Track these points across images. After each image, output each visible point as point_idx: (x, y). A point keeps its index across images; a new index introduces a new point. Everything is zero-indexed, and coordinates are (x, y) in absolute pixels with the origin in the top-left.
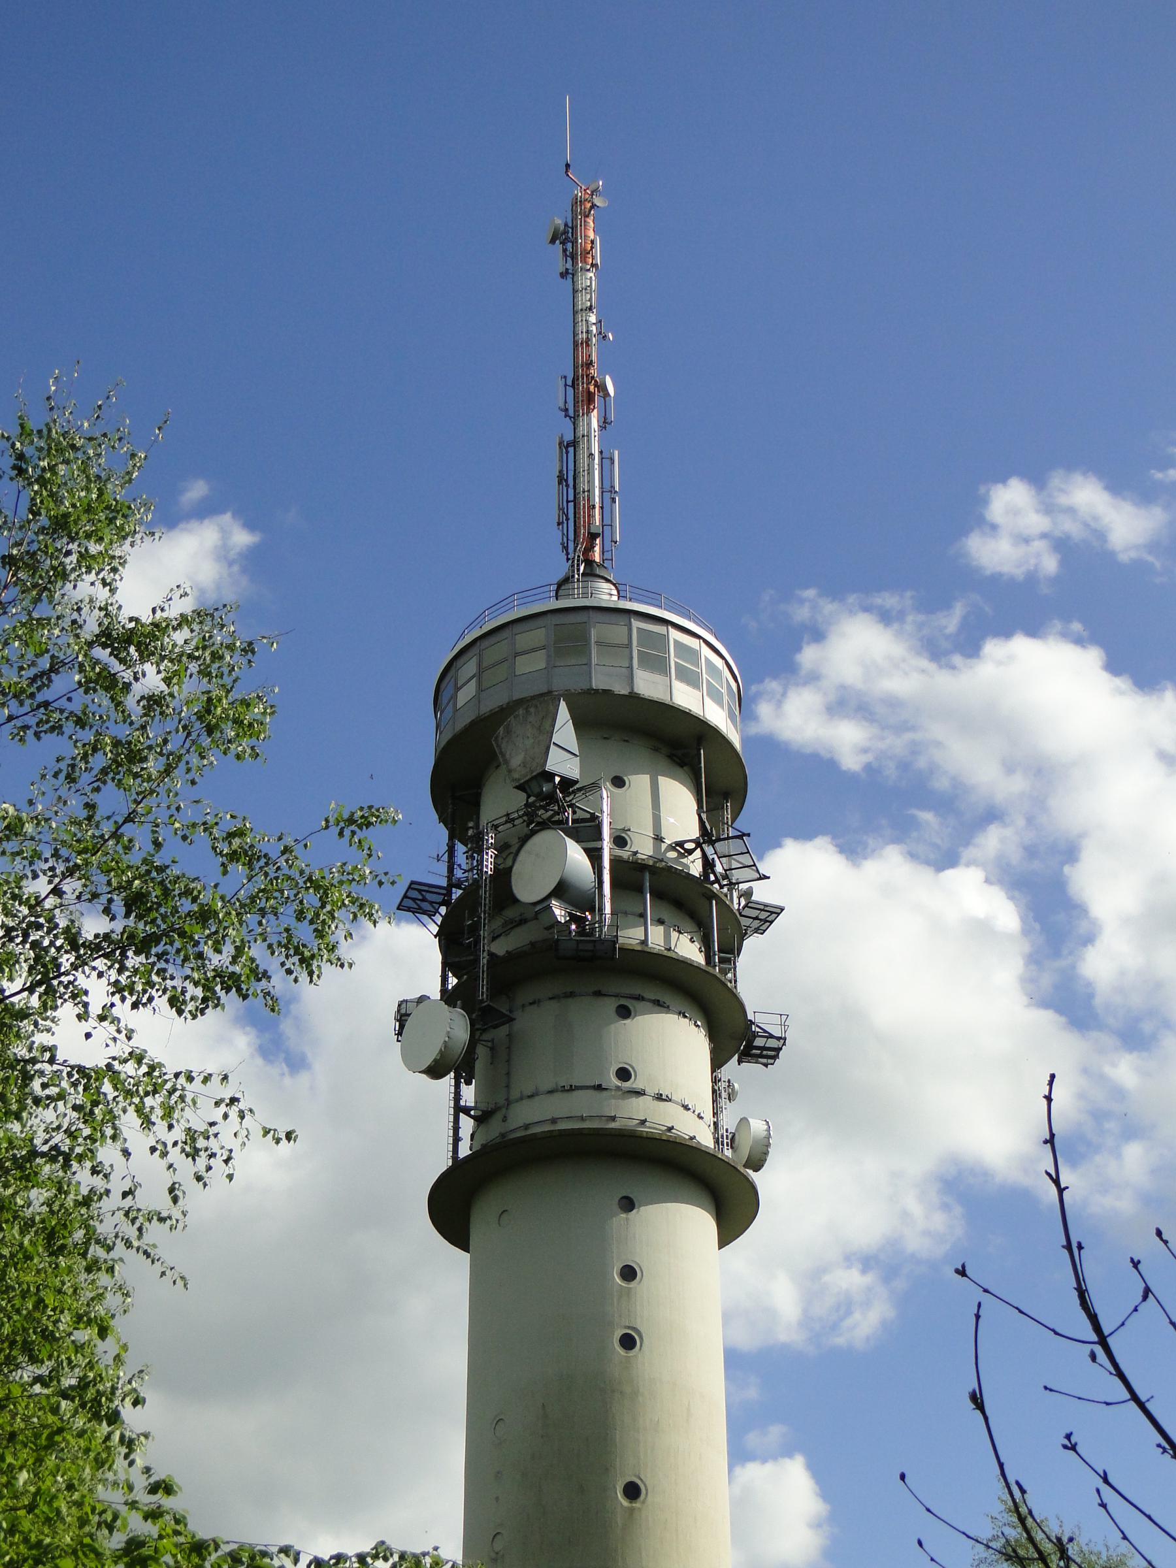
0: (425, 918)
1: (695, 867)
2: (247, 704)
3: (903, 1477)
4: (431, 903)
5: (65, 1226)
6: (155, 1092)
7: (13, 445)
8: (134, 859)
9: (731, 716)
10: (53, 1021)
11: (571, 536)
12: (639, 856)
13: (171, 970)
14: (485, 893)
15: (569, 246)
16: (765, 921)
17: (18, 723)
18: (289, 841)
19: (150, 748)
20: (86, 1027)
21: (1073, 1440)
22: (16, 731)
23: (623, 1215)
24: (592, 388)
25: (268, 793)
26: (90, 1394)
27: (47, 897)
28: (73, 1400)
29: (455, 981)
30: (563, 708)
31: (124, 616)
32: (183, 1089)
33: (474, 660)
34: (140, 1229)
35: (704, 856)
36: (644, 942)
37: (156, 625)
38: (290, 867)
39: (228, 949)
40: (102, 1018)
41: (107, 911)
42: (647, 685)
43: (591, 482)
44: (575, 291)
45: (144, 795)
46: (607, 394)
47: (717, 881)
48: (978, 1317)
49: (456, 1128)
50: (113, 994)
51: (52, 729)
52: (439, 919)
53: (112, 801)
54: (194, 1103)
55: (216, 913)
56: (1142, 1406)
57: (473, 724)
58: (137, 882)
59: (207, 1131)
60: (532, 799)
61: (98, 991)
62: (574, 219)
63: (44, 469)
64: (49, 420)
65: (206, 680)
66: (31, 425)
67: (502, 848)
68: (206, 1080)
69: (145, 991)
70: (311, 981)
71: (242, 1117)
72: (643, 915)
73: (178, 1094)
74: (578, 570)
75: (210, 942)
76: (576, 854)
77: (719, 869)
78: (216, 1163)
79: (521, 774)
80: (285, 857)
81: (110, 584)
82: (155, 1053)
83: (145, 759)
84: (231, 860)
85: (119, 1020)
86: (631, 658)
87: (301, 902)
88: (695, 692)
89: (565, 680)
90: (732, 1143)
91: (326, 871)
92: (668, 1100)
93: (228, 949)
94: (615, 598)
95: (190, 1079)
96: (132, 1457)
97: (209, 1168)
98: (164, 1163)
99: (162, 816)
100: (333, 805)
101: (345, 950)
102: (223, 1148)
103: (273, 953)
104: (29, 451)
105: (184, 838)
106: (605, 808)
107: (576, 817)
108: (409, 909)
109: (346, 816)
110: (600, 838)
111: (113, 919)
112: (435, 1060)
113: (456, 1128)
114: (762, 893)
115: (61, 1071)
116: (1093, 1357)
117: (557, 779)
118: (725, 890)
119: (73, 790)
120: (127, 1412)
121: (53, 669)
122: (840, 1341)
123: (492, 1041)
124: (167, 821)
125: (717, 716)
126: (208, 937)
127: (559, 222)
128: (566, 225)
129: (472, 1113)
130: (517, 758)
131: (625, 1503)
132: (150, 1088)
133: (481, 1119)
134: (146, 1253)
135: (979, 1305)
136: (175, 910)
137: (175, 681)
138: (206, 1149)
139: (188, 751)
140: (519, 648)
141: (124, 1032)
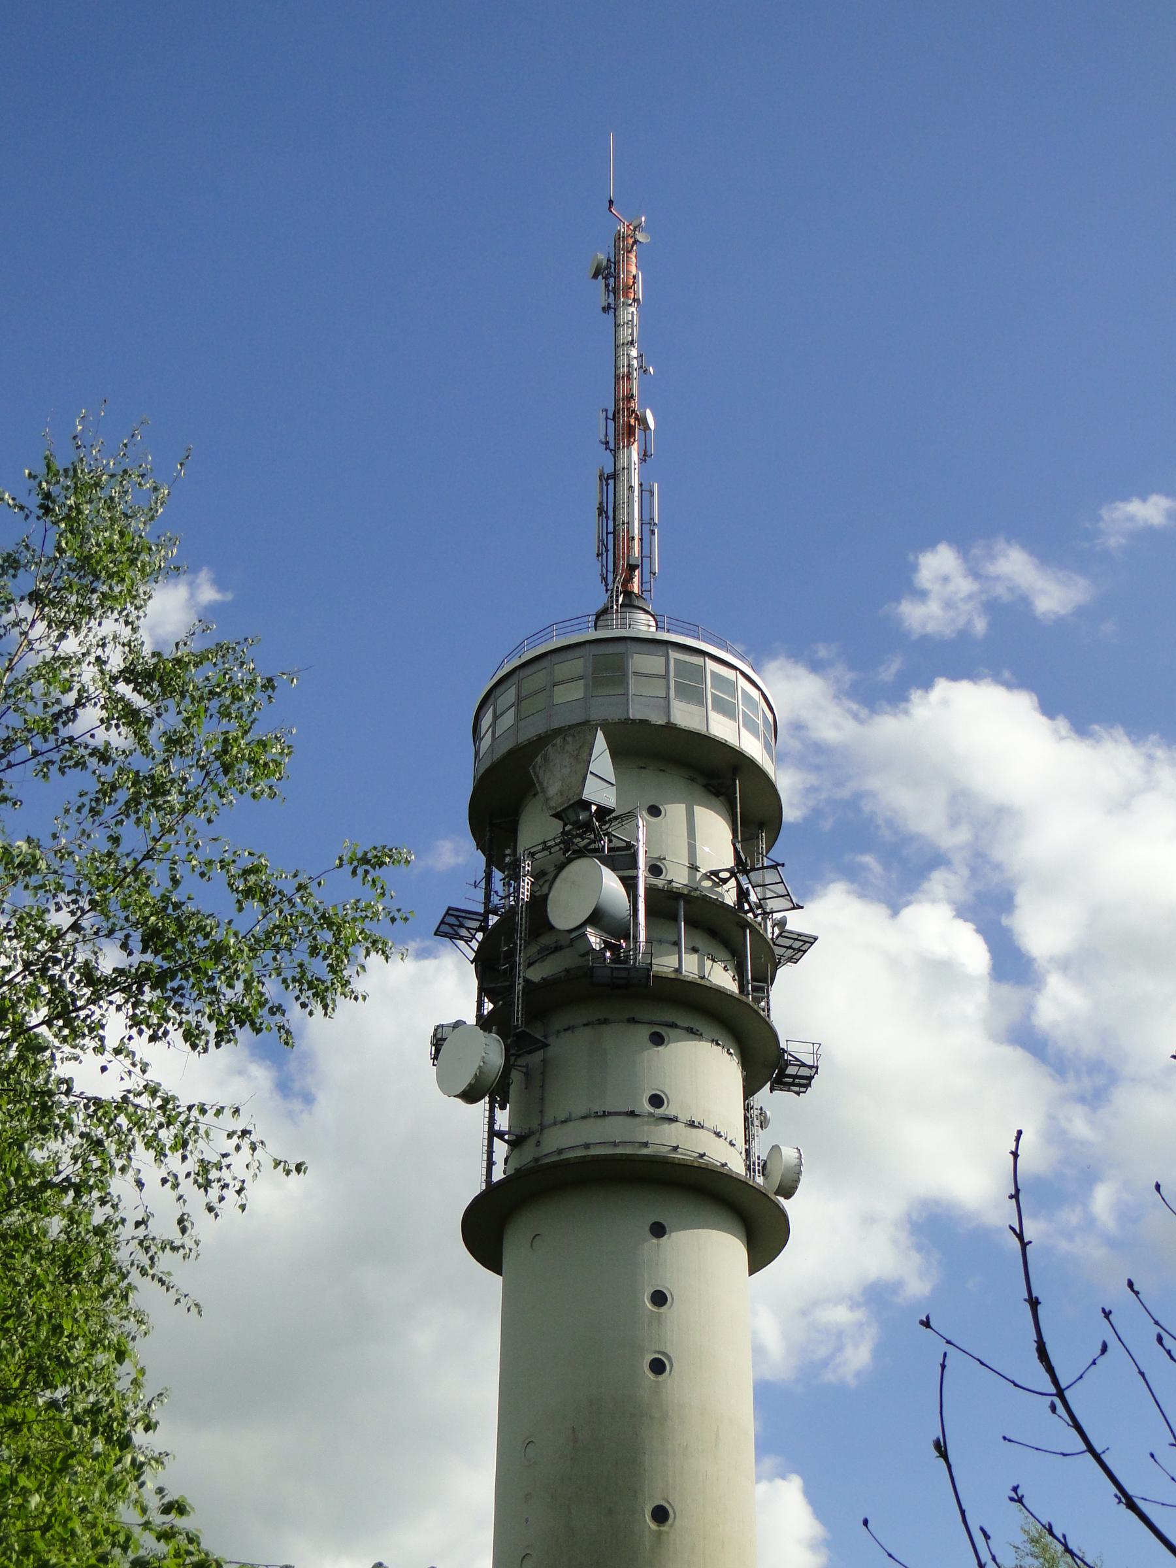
0: (461, 943)
1: (729, 896)
2: (263, 744)
3: (866, 1522)
4: (468, 929)
5: (80, 1254)
6: (169, 1124)
7: (40, 485)
8: (153, 894)
9: (767, 747)
10: (82, 1049)
11: (611, 568)
12: (674, 884)
13: (187, 1004)
14: (521, 920)
15: (612, 280)
16: (799, 950)
17: (42, 759)
18: (303, 878)
19: (173, 781)
20: (101, 1060)
21: (1020, 1492)
22: (39, 768)
23: (654, 1241)
24: (632, 422)
25: (278, 831)
26: (103, 1418)
27: (66, 932)
28: (85, 1425)
29: (491, 1006)
30: (600, 735)
31: (147, 650)
32: (197, 1121)
33: (513, 690)
34: (152, 1258)
35: (739, 885)
36: (678, 970)
37: (178, 661)
38: (305, 903)
39: (239, 986)
40: (117, 1052)
41: (124, 946)
42: (684, 715)
43: (630, 514)
44: (617, 325)
45: (165, 830)
46: (647, 428)
47: (751, 910)
48: (943, 1366)
49: (490, 1152)
50: (131, 1027)
51: (77, 764)
52: (475, 945)
53: (134, 838)
54: (207, 1134)
55: (228, 947)
56: (1097, 1457)
57: (511, 753)
58: (153, 918)
59: (220, 1162)
60: (568, 828)
61: (116, 1025)
62: (617, 254)
63: (70, 507)
64: (76, 459)
65: (224, 721)
66: (59, 464)
67: (539, 876)
68: (219, 1112)
69: (160, 1026)
70: (326, 1014)
71: (254, 1149)
72: (677, 944)
73: (191, 1126)
74: (617, 601)
75: (223, 977)
76: (611, 882)
77: (753, 898)
78: (230, 1194)
79: (558, 803)
80: (300, 894)
81: (132, 623)
82: (168, 1086)
83: (168, 792)
84: (247, 897)
85: (134, 1054)
86: (668, 688)
87: (315, 938)
88: (732, 722)
89: (604, 709)
90: (764, 1171)
91: (340, 907)
93: (239, 986)
94: (653, 629)
95: (203, 1111)
96: (142, 1478)
97: (222, 1199)
98: (174, 1195)
99: (180, 852)
100: (347, 843)
101: (358, 985)
102: (235, 1178)
103: (287, 987)
104: (55, 490)
105: (202, 875)
106: (641, 837)
107: (612, 845)
108: (446, 935)
109: (359, 855)
110: (635, 866)
111: (130, 954)
112: (470, 1085)
113: (490, 1152)
114: (796, 922)
115: (79, 1103)
116: (1053, 1408)
117: (594, 808)
118: (759, 919)
119: (97, 823)
120: (139, 1437)
121: (79, 703)
122: (829, 1377)
123: (527, 1066)
124: (185, 857)
125: (752, 747)
126: (222, 972)
127: (602, 257)
128: (609, 260)
129: (506, 1137)
130: (554, 787)
131: (653, 1526)
132: (163, 1120)
133: (515, 1144)
134: (160, 1280)
135: (945, 1355)
136: (191, 945)
137: (194, 721)
138: (219, 1180)
139: (205, 790)
140: (558, 678)
141: (139, 1066)
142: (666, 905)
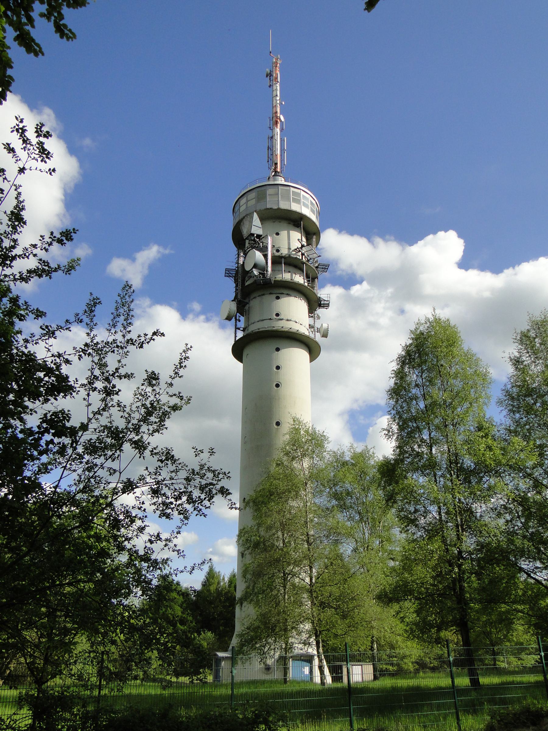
30: (255, 214)
42: (283, 205)
76: (259, 255)
92: (290, 320)
110: (267, 251)
142: (277, 261)
